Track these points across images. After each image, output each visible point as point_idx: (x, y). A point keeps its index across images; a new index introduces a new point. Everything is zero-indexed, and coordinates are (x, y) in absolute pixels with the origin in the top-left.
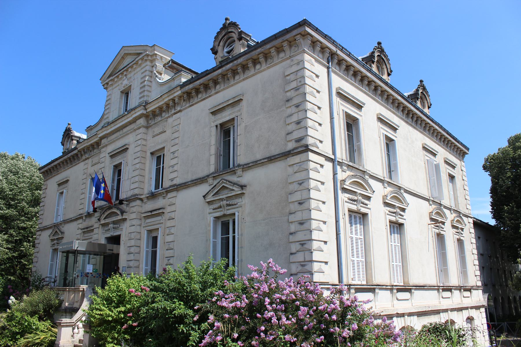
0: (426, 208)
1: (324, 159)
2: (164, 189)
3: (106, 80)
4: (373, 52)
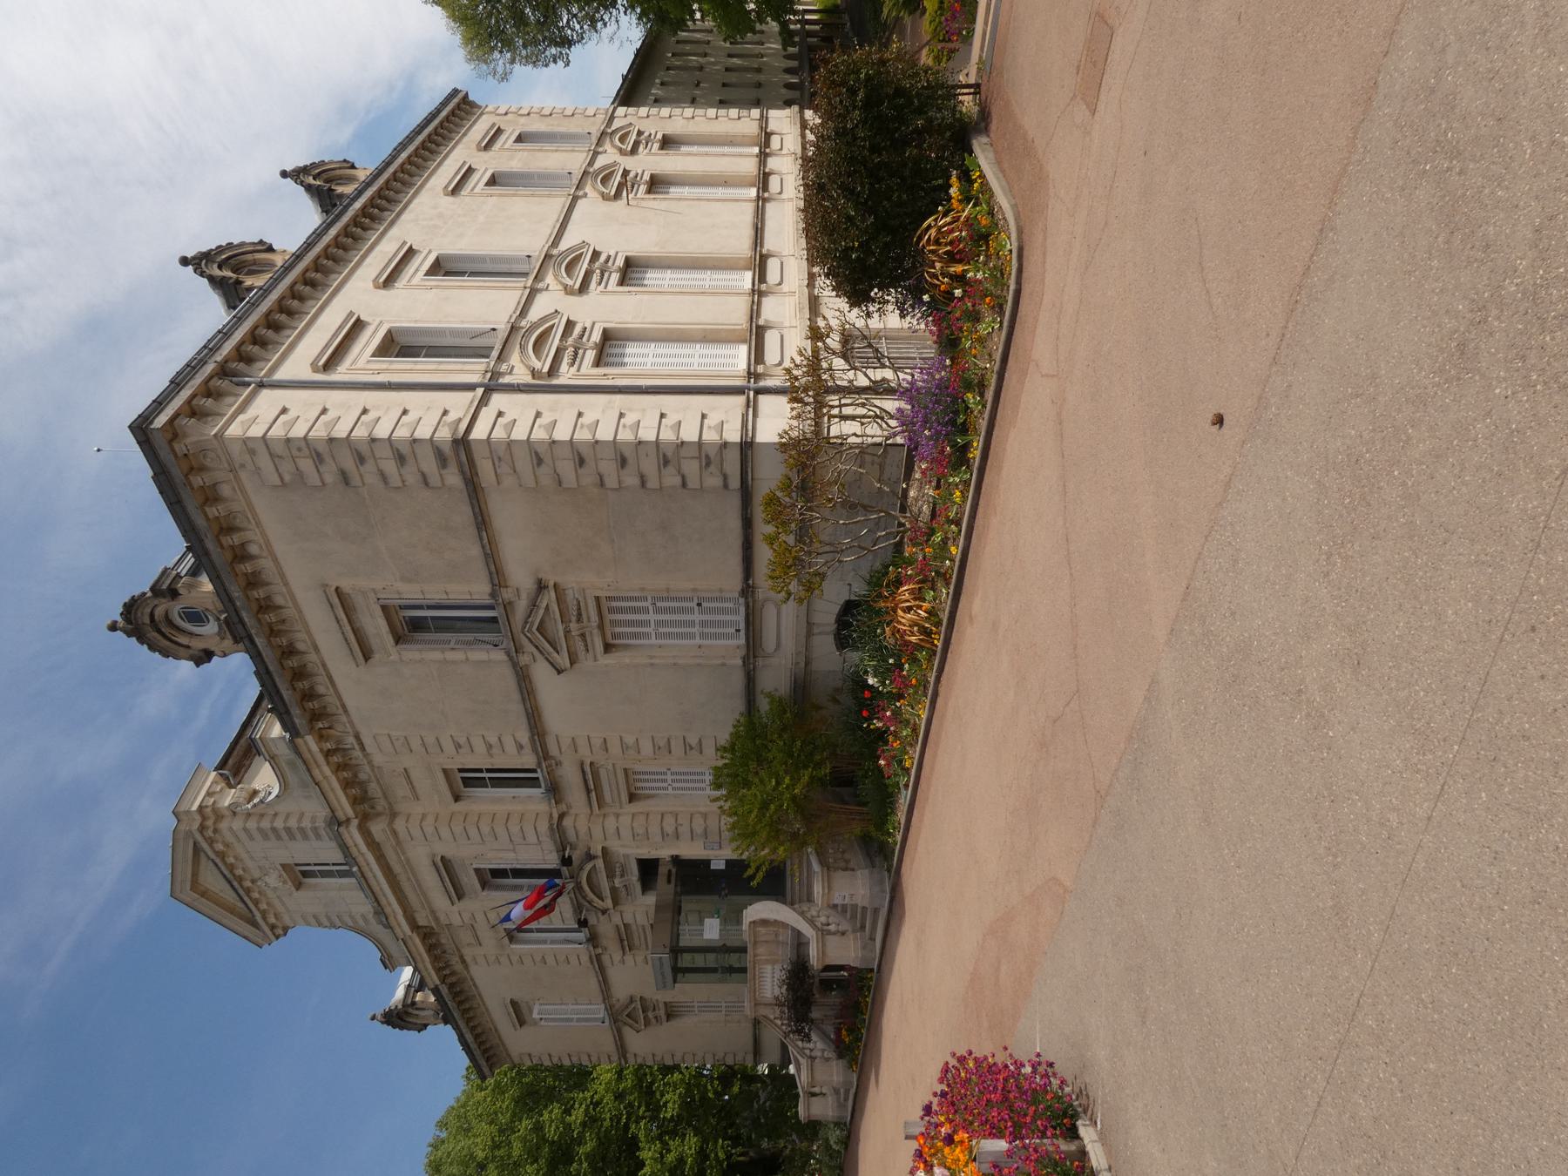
0: (591, 205)
1: (484, 408)
2: (539, 765)
3: (264, 932)
4: (212, 279)
